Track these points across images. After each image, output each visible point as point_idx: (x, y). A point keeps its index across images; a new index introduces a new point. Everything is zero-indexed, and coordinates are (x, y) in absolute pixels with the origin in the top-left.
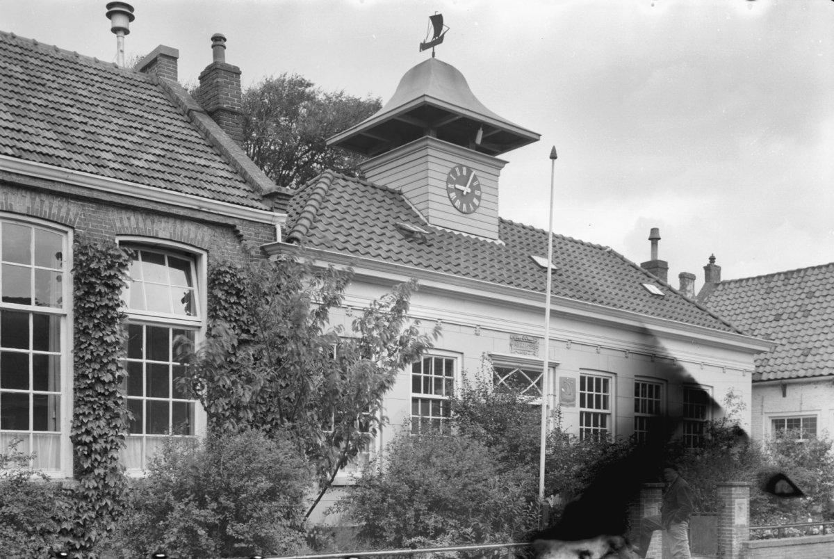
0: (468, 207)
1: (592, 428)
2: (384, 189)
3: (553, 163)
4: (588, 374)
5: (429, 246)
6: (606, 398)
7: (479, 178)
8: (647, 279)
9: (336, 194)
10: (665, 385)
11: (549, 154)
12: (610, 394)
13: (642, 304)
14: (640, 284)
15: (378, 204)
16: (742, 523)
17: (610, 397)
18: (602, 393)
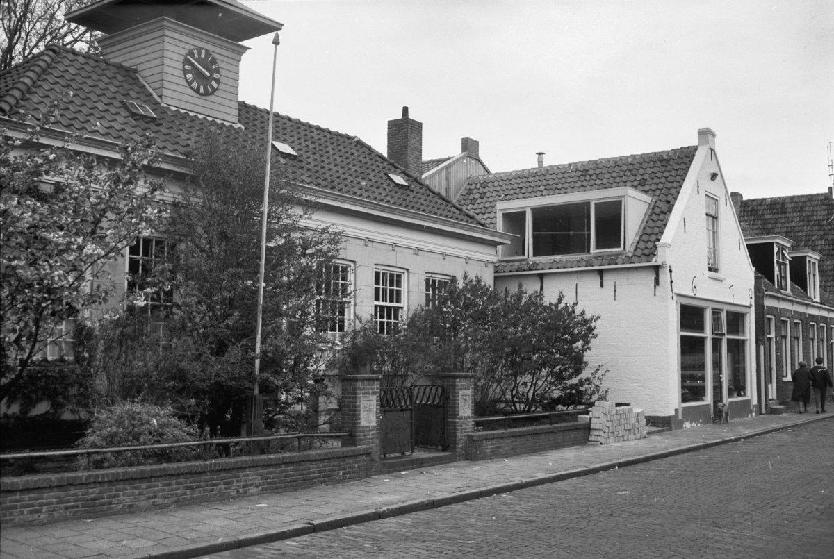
0: (205, 89)
1: (385, 320)
2: (119, 67)
3: (276, 48)
4: (381, 269)
5: (158, 125)
6: (399, 293)
7: (218, 62)
8: (393, 169)
9: (61, 67)
10: (406, 274)
11: (272, 40)
12: (402, 289)
13: (384, 193)
14: (386, 174)
15: (107, 80)
16: (466, 415)
17: (402, 292)
18: (395, 288)
